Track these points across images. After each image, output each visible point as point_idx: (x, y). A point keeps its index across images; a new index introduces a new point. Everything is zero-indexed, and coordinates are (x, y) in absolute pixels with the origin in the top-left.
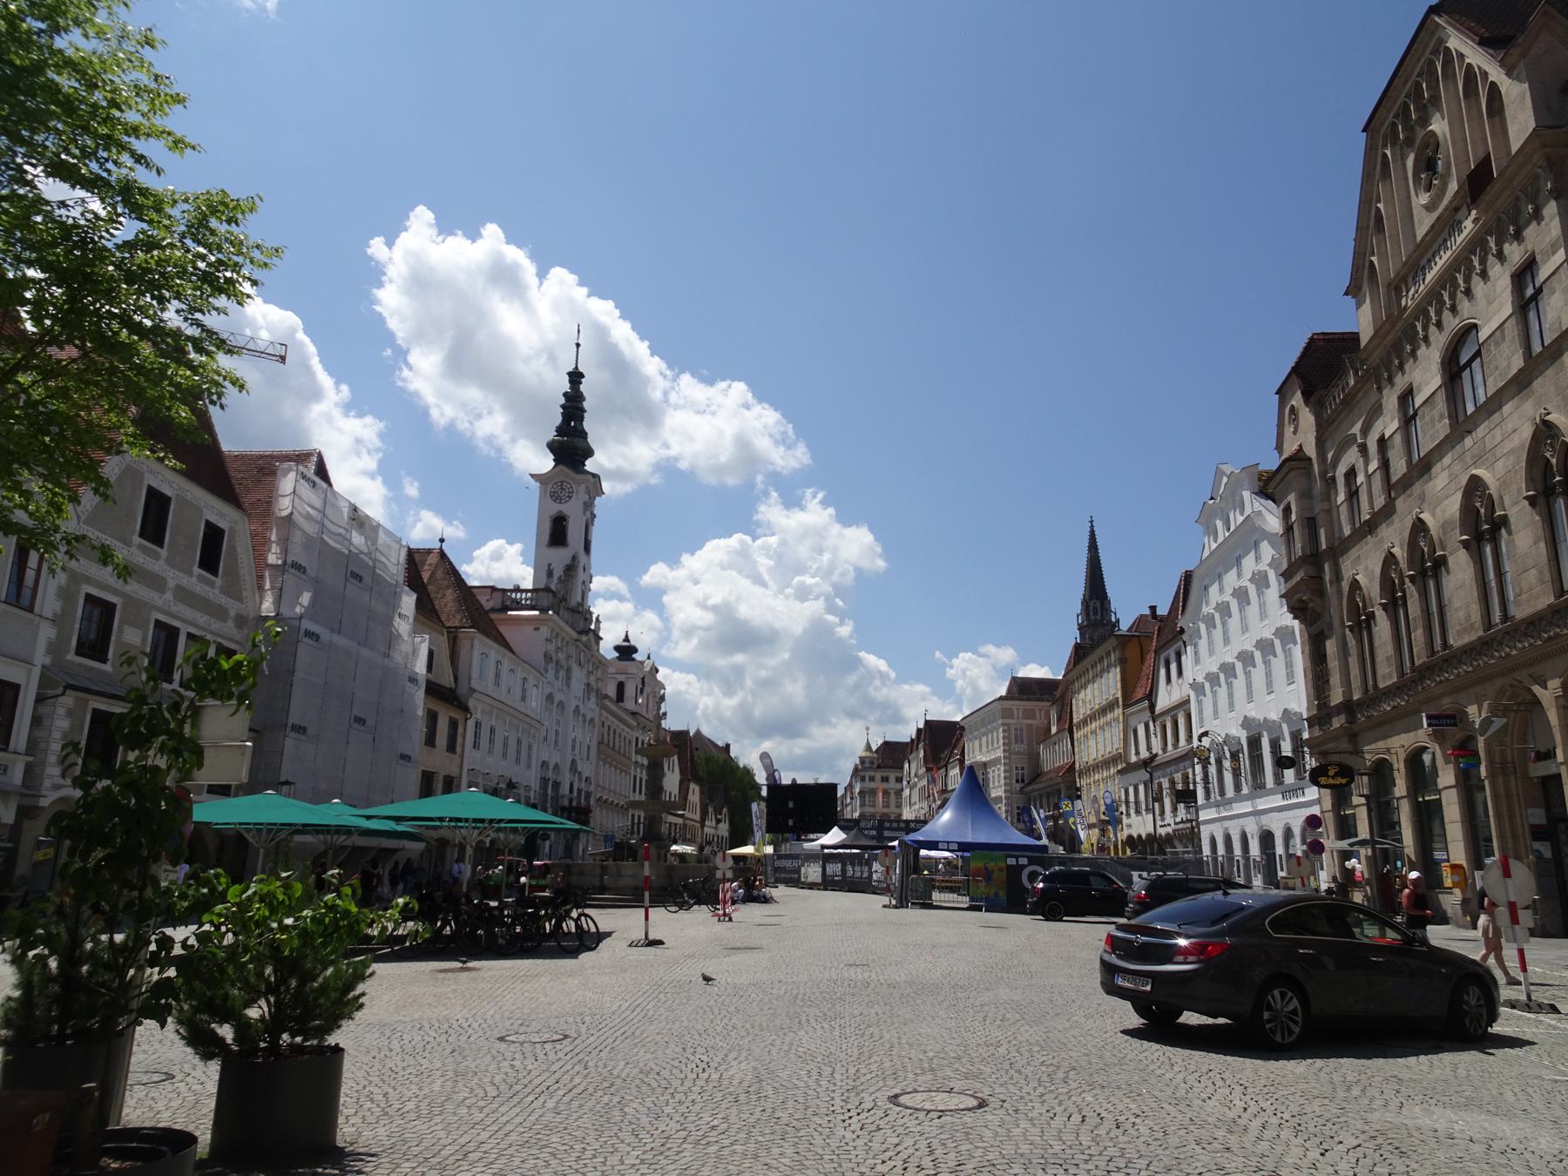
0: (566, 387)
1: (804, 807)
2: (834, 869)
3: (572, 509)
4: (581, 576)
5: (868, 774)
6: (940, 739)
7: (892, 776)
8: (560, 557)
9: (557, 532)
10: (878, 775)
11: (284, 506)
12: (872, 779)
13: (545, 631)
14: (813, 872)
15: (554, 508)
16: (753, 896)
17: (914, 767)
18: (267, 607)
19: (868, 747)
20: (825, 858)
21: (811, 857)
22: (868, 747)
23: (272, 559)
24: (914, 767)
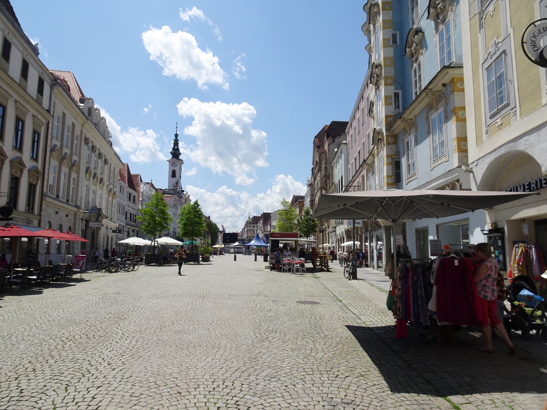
0: (174, 138)
1: (230, 238)
2: (236, 250)
3: (177, 169)
4: (179, 184)
5: (249, 225)
6: (266, 217)
7: (256, 226)
8: (174, 180)
9: (173, 174)
10: (252, 226)
11: (141, 190)
12: (250, 227)
13: (173, 199)
14: (232, 250)
15: (173, 168)
16: (206, 259)
17: (260, 224)
18: (140, 208)
19: (249, 218)
20: (235, 248)
21: (232, 248)
22: (249, 218)
23: (141, 199)
24: (260, 224)
